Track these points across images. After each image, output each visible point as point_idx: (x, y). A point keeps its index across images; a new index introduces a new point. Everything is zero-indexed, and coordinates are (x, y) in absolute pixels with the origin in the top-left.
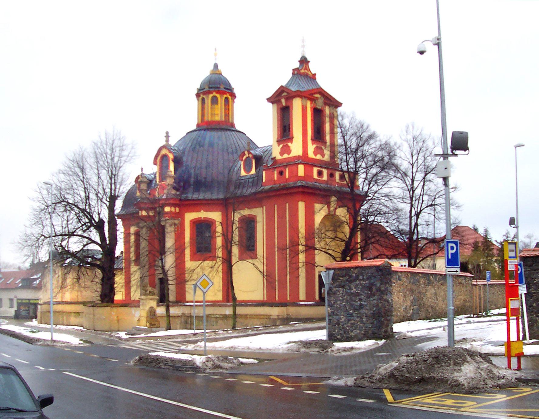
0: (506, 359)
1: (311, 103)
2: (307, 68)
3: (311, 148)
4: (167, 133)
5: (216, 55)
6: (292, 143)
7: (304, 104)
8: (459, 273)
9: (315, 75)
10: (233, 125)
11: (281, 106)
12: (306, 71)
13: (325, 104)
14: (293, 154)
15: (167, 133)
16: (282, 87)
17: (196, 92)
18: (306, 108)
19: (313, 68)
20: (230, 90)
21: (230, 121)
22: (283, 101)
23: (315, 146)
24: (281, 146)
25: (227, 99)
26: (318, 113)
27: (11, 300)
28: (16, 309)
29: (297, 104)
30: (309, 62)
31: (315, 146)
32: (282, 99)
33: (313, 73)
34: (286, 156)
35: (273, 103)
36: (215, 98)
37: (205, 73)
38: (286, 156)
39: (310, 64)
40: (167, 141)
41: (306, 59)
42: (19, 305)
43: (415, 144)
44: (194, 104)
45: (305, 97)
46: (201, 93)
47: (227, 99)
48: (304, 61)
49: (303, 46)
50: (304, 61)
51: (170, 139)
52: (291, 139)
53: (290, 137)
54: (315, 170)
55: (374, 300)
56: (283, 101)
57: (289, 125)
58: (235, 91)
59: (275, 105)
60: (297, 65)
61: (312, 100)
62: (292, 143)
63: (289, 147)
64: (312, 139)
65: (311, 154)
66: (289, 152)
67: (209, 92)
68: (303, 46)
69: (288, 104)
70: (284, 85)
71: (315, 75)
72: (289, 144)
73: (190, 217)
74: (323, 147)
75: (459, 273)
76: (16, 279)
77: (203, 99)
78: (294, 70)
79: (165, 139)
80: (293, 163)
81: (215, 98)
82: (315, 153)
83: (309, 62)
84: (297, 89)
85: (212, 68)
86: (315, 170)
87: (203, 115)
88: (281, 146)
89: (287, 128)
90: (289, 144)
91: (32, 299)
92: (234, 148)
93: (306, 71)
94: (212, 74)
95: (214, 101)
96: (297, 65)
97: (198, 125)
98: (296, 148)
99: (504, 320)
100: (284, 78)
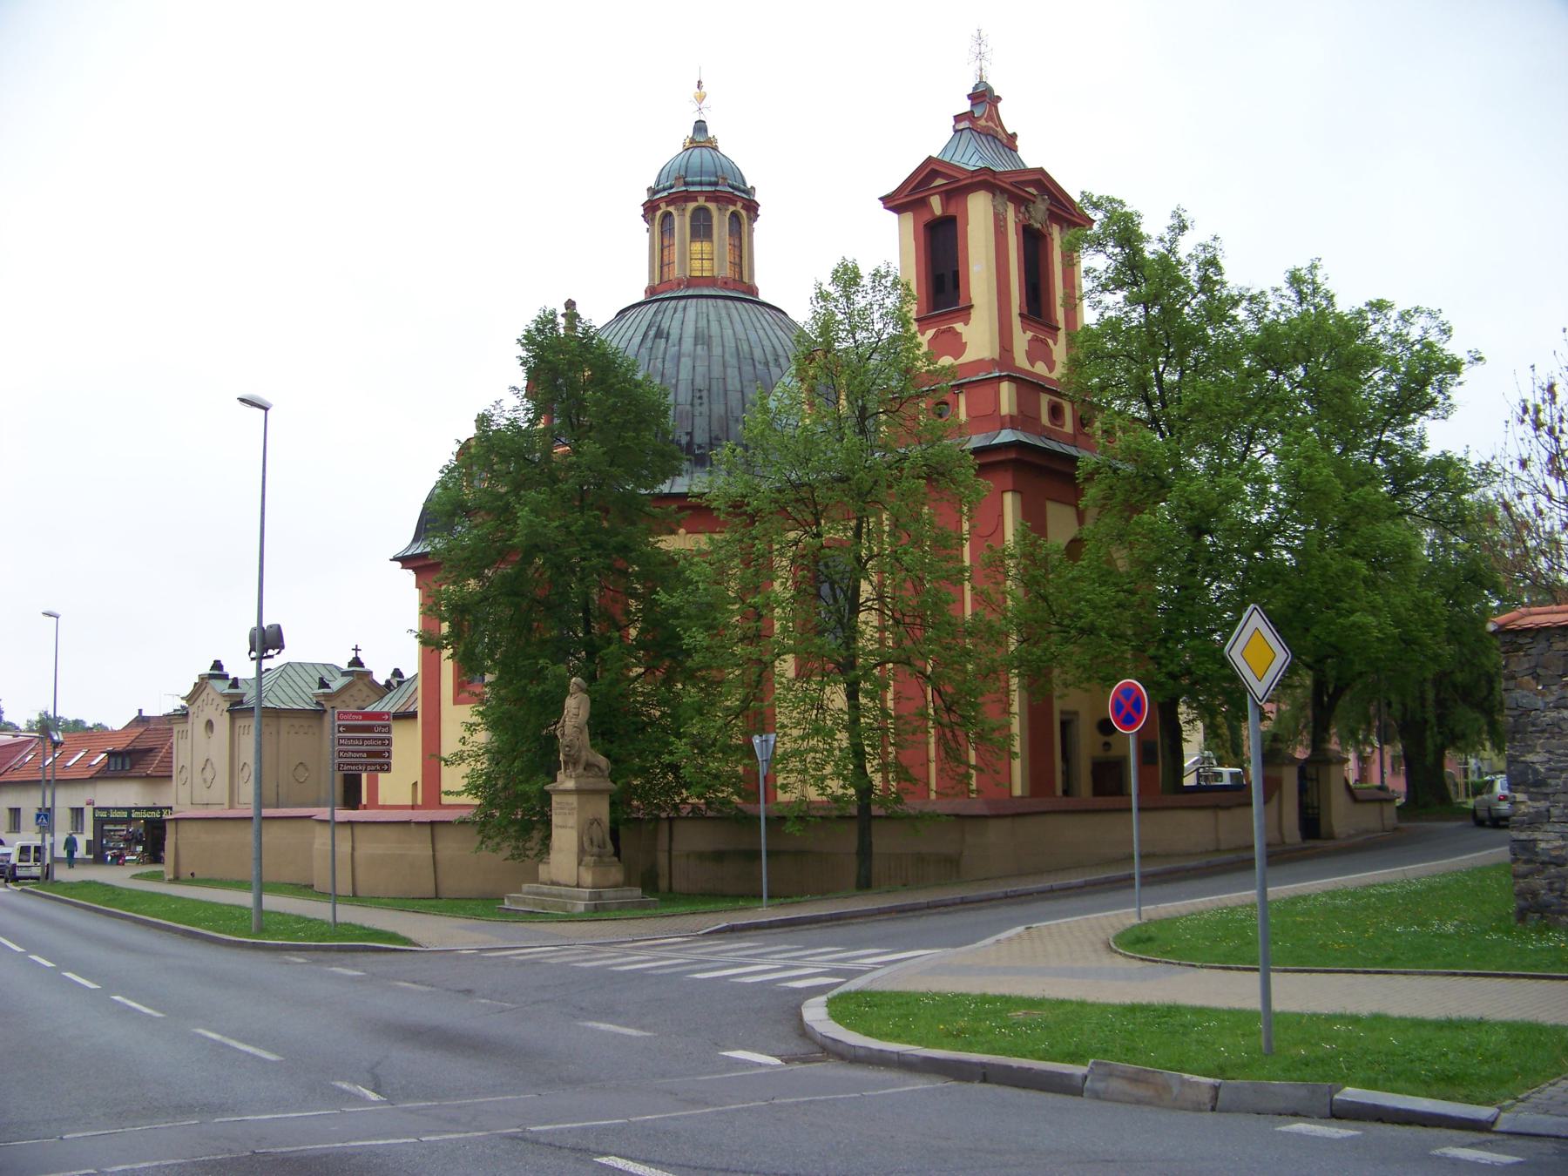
1: (1017, 211)
2: (995, 117)
3: (1021, 339)
4: (242, 400)
6: (966, 324)
7: (1001, 209)
9: (1014, 136)
10: (753, 290)
11: (927, 217)
12: (991, 124)
13: (1054, 217)
14: (969, 356)
15: (242, 400)
18: (1005, 219)
19: (1010, 117)
21: (746, 280)
22: (936, 203)
23: (1030, 334)
25: (735, 215)
26: (1034, 244)
27: (77, 813)
28: (91, 838)
29: (979, 211)
30: (999, 99)
31: (1030, 334)
32: (930, 200)
34: (946, 361)
35: (898, 209)
36: (701, 213)
39: (1000, 105)
41: (989, 90)
42: (99, 823)
44: (637, 237)
45: (1003, 191)
48: (983, 97)
49: (980, 56)
50: (983, 97)
52: (965, 312)
53: (962, 304)
54: (1045, 400)
56: (936, 203)
57: (956, 274)
59: (909, 217)
60: (966, 106)
61: (1021, 201)
62: (966, 324)
63: (958, 335)
65: (1021, 360)
66: (958, 347)
67: (688, 197)
68: (980, 56)
69: (951, 211)
71: (1014, 136)
72: (959, 327)
74: (1050, 342)
76: (90, 754)
77: (668, 215)
80: (977, 382)
81: (701, 213)
82: (1032, 357)
83: (999, 99)
84: (981, 164)
85: (689, 131)
86: (1045, 400)
88: (930, 333)
90: (959, 327)
91: (138, 809)
92: (769, 350)
93: (991, 124)
95: (701, 228)
96: (966, 106)
97: (651, 291)
98: (978, 337)
99: (448, 793)
100: (932, 137)
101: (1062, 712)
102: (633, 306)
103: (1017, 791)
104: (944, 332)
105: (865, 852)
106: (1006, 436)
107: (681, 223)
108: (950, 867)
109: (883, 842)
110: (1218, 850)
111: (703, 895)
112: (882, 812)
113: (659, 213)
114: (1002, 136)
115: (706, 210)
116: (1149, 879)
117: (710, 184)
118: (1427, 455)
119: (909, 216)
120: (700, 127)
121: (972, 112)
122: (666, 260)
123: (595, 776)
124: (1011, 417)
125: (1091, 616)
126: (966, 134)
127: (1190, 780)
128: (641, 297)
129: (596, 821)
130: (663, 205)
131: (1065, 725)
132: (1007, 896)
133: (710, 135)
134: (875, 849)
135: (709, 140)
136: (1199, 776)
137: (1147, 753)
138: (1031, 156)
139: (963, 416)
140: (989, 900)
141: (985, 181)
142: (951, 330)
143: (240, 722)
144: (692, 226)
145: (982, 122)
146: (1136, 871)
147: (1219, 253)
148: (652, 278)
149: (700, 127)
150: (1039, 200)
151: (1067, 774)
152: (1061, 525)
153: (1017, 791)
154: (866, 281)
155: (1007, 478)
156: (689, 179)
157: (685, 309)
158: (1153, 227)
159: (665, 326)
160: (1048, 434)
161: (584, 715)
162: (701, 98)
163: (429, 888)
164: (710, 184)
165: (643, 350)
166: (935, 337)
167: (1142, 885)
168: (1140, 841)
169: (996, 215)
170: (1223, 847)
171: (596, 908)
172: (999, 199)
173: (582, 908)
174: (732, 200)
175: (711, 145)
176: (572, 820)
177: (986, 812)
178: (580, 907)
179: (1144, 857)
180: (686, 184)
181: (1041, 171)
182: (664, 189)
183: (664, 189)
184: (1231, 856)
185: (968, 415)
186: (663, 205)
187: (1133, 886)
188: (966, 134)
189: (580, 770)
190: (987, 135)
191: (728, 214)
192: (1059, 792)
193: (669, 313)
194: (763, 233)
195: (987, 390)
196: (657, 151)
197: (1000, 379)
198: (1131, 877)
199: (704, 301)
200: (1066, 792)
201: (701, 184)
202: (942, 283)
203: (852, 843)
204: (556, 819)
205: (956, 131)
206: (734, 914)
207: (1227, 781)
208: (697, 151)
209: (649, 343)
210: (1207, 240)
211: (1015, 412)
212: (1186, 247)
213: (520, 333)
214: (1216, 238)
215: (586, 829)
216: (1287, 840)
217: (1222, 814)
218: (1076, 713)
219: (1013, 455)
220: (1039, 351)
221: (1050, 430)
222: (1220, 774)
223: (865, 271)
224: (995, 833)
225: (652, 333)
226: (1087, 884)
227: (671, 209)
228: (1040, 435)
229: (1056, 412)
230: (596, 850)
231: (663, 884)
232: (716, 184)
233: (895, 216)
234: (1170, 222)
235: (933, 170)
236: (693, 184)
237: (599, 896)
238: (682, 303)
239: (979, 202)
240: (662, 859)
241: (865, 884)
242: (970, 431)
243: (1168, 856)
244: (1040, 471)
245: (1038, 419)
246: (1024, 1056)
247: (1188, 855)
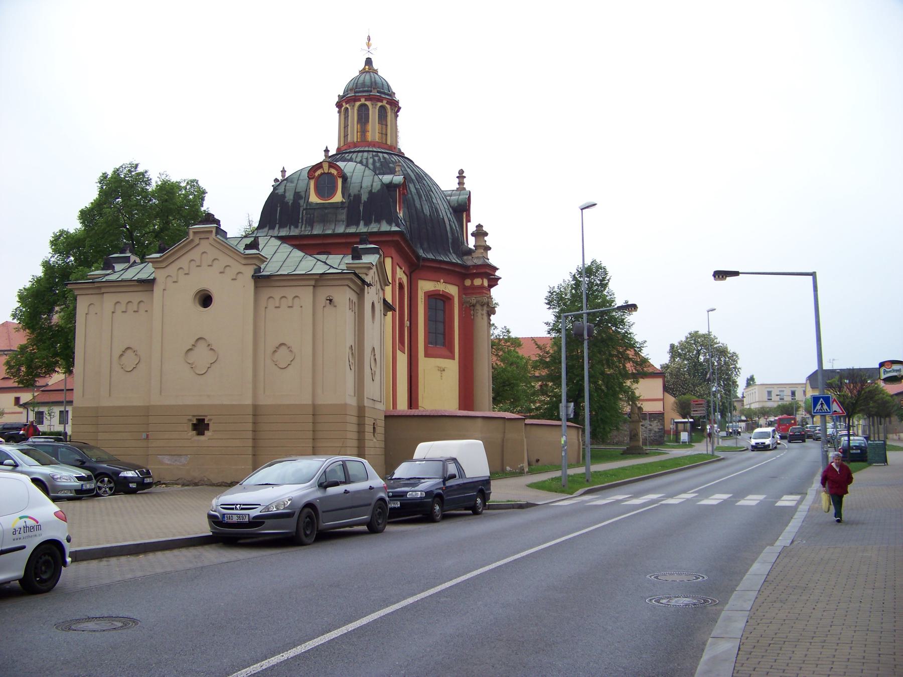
4: (461, 172)
5: (369, 45)
8: (351, 261)
15: (461, 172)
17: (337, 100)
20: (390, 95)
25: (382, 108)
37: (352, 70)
40: (461, 183)
47: (382, 109)
51: (465, 180)
55: (485, 308)
58: (398, 97)
73: (425, 286)
75: (351, 261)
79: (457, 181)
81: (363, 109)
85: (361, 65)
87: (346, 136)
94: (363, 72)
115: (365, 105)
118: (151, 188)
120: (369, 62)
130: (385, 102)
143: (266, 293)
144: (359, 115)
149: (369, 62)
162: (369, 45)
174: (380, 99)
175: (376, 72)
194: (404, 122)
227: (368, 103)
246: (295, 646)
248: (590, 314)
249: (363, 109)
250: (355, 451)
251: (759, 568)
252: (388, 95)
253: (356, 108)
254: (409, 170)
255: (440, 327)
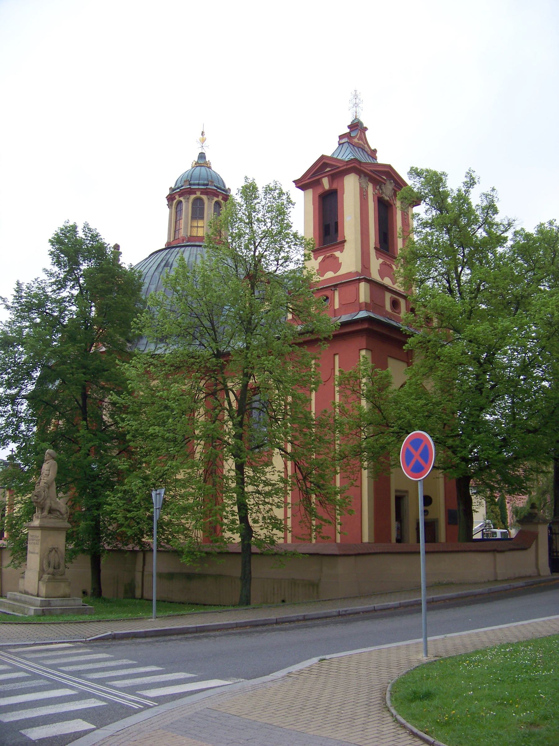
0: (238, 562)
3: (376, 263)
6: (342, 252)
9: (375, 151)
11: (320, 191)
12: (360, 142)
14: (343, 271)
16: (323, 157)
17: (168, 193)
18: (367, 192)
22: (326, 182)
23: (381, 261)
24: (320, 258)
26: (385, 209)
29: (351, 185)
30: (366, 129)
31: (381, 261)
33: (373, 148)
34: (330, 275)
38: (330, 275)
39: (367, 133)
43: (207, 476)
44: (164, 212)
45: (366, 175)
46: (174, 197)
47: (218, 204)
48: (357, 127)
49: (356, 105)
54: (388, 297)
56: (326, 182)
57: (336, 224)
61: (376, 183)
62: (342, 252)
63: (337, 258)
64: (376, 248)
66: (337, 266)
67: (191, 192)
68: (356, 105)
69: (334, 187)
70: (329, 154)
72: (337, 254)
78: (341, 137)
81: (198, 203)
82: (382, 274)
83: (366, 129)
84: (353, 157)
88: (320, 258)
89: (332, 229)
90: (337, 254)
93: (360, 142)
94: (197, 165)
98: (348, 260)
101: (396, 491)
102: (156, 252)
103: (366, 539)
104: (328, 257)
105: (246, 578)
106: (363, 314)
107: (187, 206)
108: (312, 590)
109: (261, 570)
110: (496, 580)
111: (180, 603)
112: (258, 551)
113: (175, 202)
114: (367, 149)
116: (433, 605)
117: (204, 185)
119: (310, 192)
120: (202, 156)
121: (349, 133)
122: (178, 228)
123: (57, 518)
124: (366, 303)
125: (409, 416)
126: (346, 145)
127: (478, 536)
128: (164, 247)
129: (54, 550)
130: (177, 197)
131: (399, 499)
132: (339, 615)
133: (207, 160)
134: (253, 575)
135: (206, 163)
136: (483, 534)
137: (451, 517)
138: (382, 159)
139: (337, 306)
140: (265, 623)
141: (354, 167)
142: (332, 256)
144: (192, 208)
145: (356, 140)
146: (423, 597)
147: (495, 199)
148: (169, 237)
149: (202, 156)
150: (388, 183)
151: (400, 530)
152: (397, 373)
153: (366, 539)
154: (261, 192)
155: (362, 341)
156: (192, 182)
157: (184, 251)
158: (453, 184)
159: (171, 261)
160: (386, 315)
161: (53, 474)
162: (203, 141)
163: (36, 594)
164: (204, 185)
165: (156, 273)
166: (323, 260)
167: (428, 609)
168: (427, 575)
169: (361, 189)
170: (499, 579)
171: (44, 613)
172: (364, 180)
173: (32, 613)
176: (37, 549)
177: (338, 553)
178: (31, 610)
179: (429, 587)
180: (190, 184)
181: (389, 167)
182: (178, 188)
183: (178, 188)
184: (505, 585)
185: (340, 304)
186: (177, 197)
187: (420, 611)
188: (346, 145)
189: (46, 513)
190: (358, 148)
191: (213, 202)
192: (394, 540)
193: (174, 254)
195: (352, 288)
196: (177, 168)
197: (360, 280)
198: (419, 604)
199: (195, 248)
200: (398, 541)
201: (199, 185)
202: (328, 232)
203: (237, 572)
204: (30, 547)
205: (340, 144)
206: (133, 624)
207: (499, 536)
208: (198, 168)
209: (160, 269)
210: (487, 190)
211: (368, 301)
212: (476, 199)
213: (51, 236)
214: (493, 190)
215: (48, 555)
216: (542, 574)
217: (499, 556)
218: (407, 492)
219: (366, 326)
220: (385, 270)
221: (391, 314)
222: (495, 533)
223: (260, 186)
224: (343, 567)
225: (163, 264)
226: (401, 606)
227: (181, 199)
228: (384, 316)
229: (395, 304)
230: (51, 570)
231: (138, 593)
232: (207, 185)
233: (303, 192)
234: (466, 180)
235: (324, 163)
236: (194, 185)
237: (49, 604)
238: (183, 249)
239: (347, 175)
240: (138, 576)
241: (245, 601)
242: (338, 312)
243: (461, 584)
244: (382, 336)
245: (384, 307)
247: (475, 583)
248: (349, 127)
249: (198, 203)
250: (437, 465)
251: (388, 696)
252: (223, 190)
253: (191, 201)
254: (200, 187)
255: (497, 509)
